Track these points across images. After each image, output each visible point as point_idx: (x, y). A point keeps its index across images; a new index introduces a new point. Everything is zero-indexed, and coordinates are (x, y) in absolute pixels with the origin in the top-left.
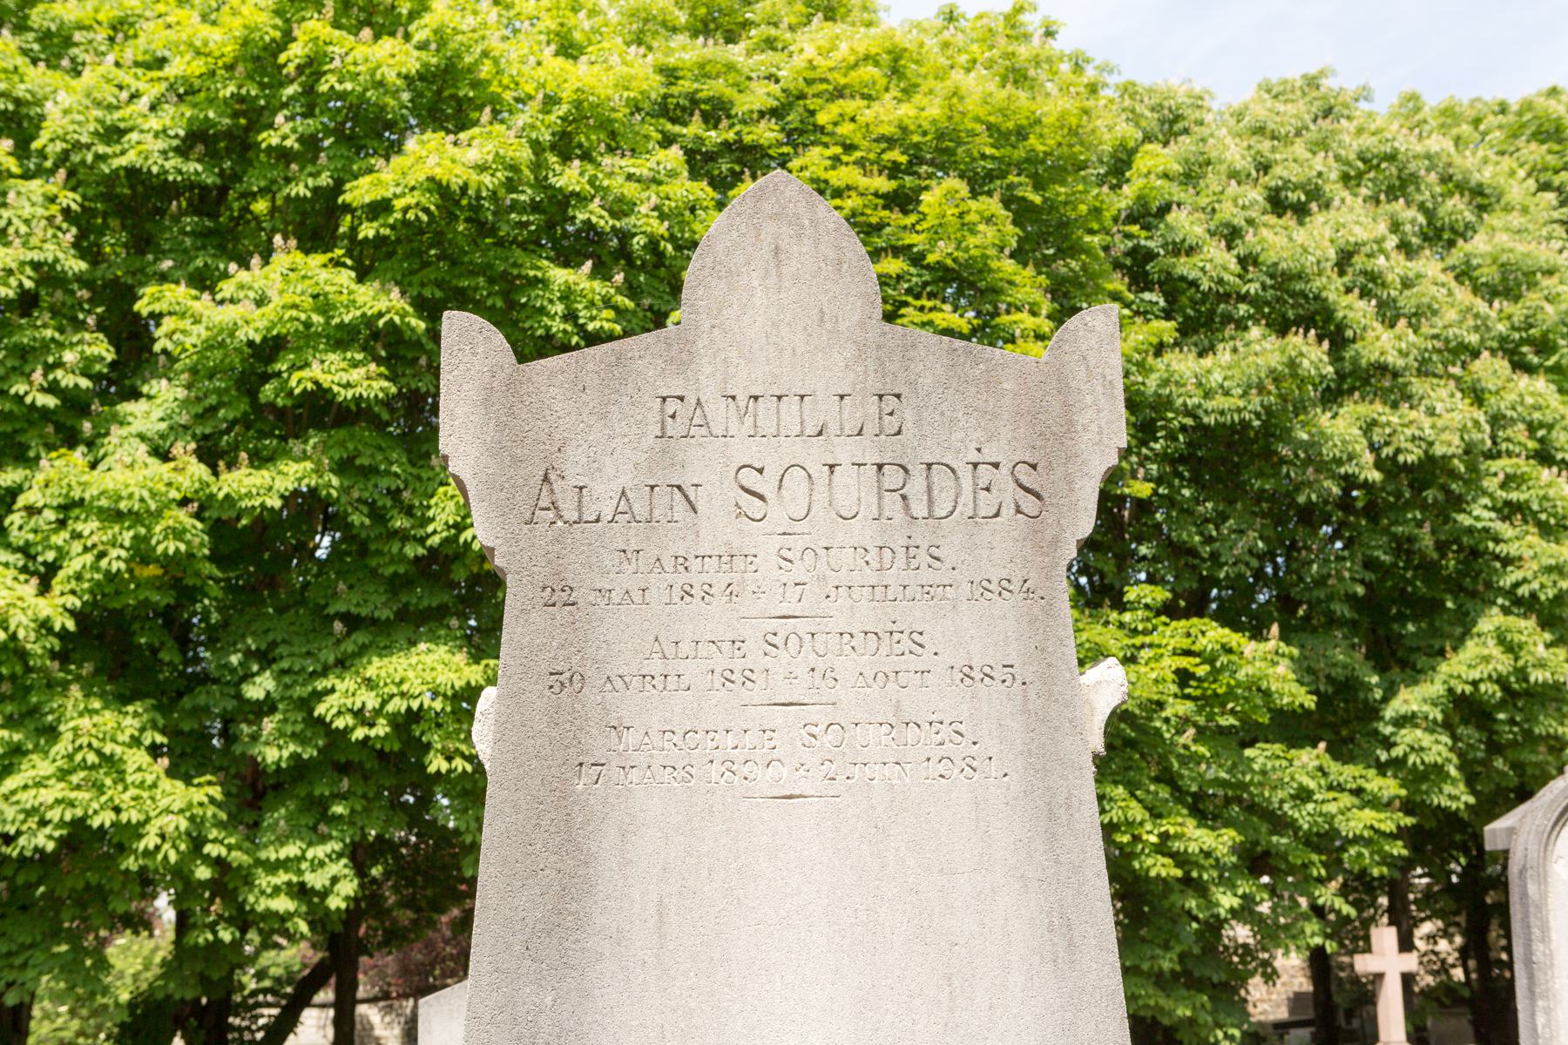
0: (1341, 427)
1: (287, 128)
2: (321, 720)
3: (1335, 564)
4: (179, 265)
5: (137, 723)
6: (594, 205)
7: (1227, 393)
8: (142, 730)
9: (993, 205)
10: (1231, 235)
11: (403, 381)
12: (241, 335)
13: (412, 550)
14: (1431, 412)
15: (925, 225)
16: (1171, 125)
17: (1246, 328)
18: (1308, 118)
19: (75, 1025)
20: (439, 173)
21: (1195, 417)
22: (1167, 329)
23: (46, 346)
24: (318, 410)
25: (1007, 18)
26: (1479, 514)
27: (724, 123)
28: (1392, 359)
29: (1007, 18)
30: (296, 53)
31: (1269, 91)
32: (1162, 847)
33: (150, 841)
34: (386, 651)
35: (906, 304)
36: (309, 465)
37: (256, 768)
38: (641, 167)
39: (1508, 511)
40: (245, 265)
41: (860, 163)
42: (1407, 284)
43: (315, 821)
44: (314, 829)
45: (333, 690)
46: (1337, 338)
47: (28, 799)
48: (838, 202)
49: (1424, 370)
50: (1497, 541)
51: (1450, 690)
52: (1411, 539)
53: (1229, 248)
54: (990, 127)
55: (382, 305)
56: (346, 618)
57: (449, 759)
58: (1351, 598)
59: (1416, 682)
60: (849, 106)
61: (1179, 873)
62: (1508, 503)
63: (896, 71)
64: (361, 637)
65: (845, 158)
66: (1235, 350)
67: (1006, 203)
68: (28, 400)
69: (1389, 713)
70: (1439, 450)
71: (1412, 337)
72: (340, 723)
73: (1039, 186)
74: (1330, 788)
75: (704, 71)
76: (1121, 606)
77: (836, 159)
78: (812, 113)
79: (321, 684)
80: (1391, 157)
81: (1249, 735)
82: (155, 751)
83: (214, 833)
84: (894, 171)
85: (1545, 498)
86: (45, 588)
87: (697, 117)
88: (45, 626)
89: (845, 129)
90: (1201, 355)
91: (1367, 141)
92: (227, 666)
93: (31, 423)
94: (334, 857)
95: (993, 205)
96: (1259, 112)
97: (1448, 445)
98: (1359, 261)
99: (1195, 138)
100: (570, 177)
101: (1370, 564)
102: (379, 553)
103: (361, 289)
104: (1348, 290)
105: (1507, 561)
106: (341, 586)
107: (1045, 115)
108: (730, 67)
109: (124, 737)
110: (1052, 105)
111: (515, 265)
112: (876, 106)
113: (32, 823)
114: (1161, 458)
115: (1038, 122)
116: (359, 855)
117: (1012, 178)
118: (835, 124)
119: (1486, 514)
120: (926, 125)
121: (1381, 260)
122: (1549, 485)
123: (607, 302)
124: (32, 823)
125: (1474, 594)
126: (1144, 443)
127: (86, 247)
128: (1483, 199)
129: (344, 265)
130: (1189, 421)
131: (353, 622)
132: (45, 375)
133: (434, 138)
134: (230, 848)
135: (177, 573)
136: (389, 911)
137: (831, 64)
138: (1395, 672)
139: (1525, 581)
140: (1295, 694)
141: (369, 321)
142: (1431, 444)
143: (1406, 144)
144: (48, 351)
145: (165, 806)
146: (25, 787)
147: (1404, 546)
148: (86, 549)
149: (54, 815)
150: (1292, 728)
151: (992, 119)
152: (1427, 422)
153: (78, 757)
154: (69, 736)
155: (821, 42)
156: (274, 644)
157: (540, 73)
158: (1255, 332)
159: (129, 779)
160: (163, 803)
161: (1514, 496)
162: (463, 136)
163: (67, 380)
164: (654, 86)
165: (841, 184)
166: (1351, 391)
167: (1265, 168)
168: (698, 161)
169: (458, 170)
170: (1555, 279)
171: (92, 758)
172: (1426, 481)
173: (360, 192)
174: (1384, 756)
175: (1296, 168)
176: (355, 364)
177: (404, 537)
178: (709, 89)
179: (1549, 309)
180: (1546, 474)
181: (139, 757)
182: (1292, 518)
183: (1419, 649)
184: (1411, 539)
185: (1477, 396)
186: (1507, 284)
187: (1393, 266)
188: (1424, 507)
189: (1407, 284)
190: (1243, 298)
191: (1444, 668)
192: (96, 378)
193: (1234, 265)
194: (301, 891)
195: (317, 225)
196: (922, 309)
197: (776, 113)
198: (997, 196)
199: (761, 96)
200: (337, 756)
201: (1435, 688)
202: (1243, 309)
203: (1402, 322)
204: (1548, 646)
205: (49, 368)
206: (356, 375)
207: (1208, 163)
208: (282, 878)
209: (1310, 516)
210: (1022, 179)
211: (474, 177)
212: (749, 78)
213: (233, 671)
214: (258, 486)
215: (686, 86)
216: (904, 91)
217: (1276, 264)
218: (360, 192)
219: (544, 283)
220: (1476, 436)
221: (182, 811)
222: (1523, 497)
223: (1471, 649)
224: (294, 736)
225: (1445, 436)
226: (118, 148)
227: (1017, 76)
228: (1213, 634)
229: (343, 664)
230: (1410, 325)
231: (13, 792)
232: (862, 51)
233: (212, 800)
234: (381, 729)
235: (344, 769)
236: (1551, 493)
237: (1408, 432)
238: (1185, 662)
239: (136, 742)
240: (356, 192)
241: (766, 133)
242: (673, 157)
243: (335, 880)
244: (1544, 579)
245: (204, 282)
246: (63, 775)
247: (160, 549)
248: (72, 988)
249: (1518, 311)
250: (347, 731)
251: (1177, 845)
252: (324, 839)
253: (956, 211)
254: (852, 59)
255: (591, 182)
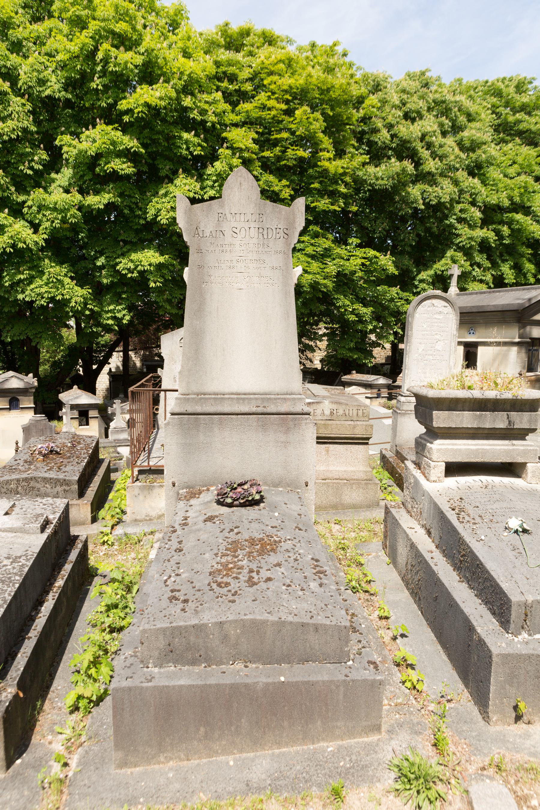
0: (415, 191)
1: (98, 82)
2: (118, 271)
3: (409, 233)
4: (67, 129)
5: (66, 270)
6: (195, 112)
7: (382, 179)
8: (67, 272)
9: (318, 115)
10: (390, 127)
11: (138, 168)
12: (89, 153)
13: (142, 222)
14: (442, 188)
15: (296, 121)
16: (377, 88)
17: (390, 159)
18: (419, 87)
19: (48, 355)
20: (148, 100)
21: (373, 187)
22: (366, 158)
23: (28, 154)
24: (114, 177)
25: (331, 47)
26: (452, 220)
27: (235, 83)
28: (433, 170)
29: (331, 47)
30: (100, 55)
31: (409, 76)
32: (352, 313)
33: (73, 304)
34: (135, 251)
35: (289, 148)
36: (112, 195)
37: (100, 283)
38: (209, 98)
39: (460, 220)
40: (87, 129)
41: (277, 99)
42: (441, 146)
43: (118, 300)
44: (118, 301)
45: (121, 262)
46: (417, 164)
47: (37, 290)
48: (269, 112)
49: (442, 175)
50: (456, 229)
51: (436, 273)
52: (431, 228)
53: (388, 132)
54: (318, 88)
55: (131, 145)
56: (123, 241)
57: (155, 283)
58: (411, 246)
59: (426, 270)
60: (275, 78)
61: (357, 319)
62: (460, 218)
63: (289, 66)
64: (128, 247)
65: (272, 97)
66: (386, 166)
67: (322, 114)
68: (25, 172)
69: (418, 278)
70: (443, 200)
71: (440, 164)
72: (124, 272)
73: (332, 109)
74: (399, 298)
75: (230, 64)
76: (346, 244)
77: (269, 97)
78: (262, 80)
79: (118, 260)
80: (444, 102)
81: (379, 282)
82: (72, 278)
83: (90, 302)
84: (287, 102)
85: (472, 216)
86: (36, 232)
87: (226, 80)
88: (36, 243)
89: (273, 87)
90: (376, 167)
91: (437, 96)
92: (90, 255)
93: (26, 179)
94: (124, 309)
95: (318, 115)
96: (404, 84)
97: (446, 199)
98: (427, 138)
99: (384, 92)
100: (187, 101)
101: (418, 235)
102: (132, 222)
103: (124, 137)
104: (423, 147)
105: (458, 235)
106: (122, 232)
107: (336, 84)
108: (238, 62)
109: (62, 274)
110: (338, 80)
111: (171, 131)
112: (283, 79)
113: (39, 298)
114: (362, 199)
115: (333, 87)
116: (130, 308)
117: (324, 106)
118: (270, 84)
119: (454, 221)
120: (298, 86)
121: (434, 138)
122: (473, 212)
123: (199, 145)
124: (39, 298)
125: (447, 245)
126: (356, 194)
127: (37, 122)
128: (470, 118)
129: (118, 130)
130: (370, 188)
131: (126, 242)
132: (29, 164)
133: (145, 86)
134: (94, 306)
135: (75, 228)
136: (136, 325)
137: (269, 63)
138: (421, 267)
139: (462, 242)
140: (392, 269)
141: (128, 150)
142: (440, 198)
143: (449, 97)
144: (30, 156)
145: (77, 294)
146: (36, 287)
147: (428, 230)
148: (48, 220)
149: (46, 295)
150: (391, 280)
151: (319, 85)
152: (440, 191)
153: (51, 280)
154: (47, 273)
155: (266, 54)
156: (103, 249)
157: (178, 65)
158: (393, 160)
159: (66, 287)
160: (76, 294)
161: (463, 216)
162: (154, 86)
163: (36, 167)
164: (212, 69)
165: (271, 106)
166: (419, 181)
167: (404, 104)
168: (227, 96)
169: (154, 100)
170: (486, 146)
171: (55, 280)
172: (438, 210)
173: (123, 105)
174: (415, 291)
175: (414, 105)
176: (124, 163)
177: (139, 217)
178: (231, 70)
179: (484, 156)
180: (473, 209)
181: (67, 280)
182: (397, 221)
183: (429, 260)
184: (431, 228)
185: (456, 183)
186: (472, 147)
187: (437, 140)
188: (436, 218)
189: (441, 146)
190: (390, 149)
191: (435, 266)
192: (43, 165)
193: (389, 137)
194: (114, 318)
195: (111, 116)
196: (293, 150)
197: (251, 79)
198: (320, 112)
199: (245, 74)
200: (122, 282)
201: (431, 272)
202: (390, 152)
203: (437, 159)
204: (464, 261)
205: (30, 162)
206: (124, 166)
207: (386, 102)
208: (110, 315)
209: (404, 220)
210: (328, 107)
211: (159, 102)
212: (243, 66)
213: (92, 256)
214: (97, 201)
215: (224, 69)
216: (292, 74)
217: (402, 137)
218: (123, 105)
219: (180, 138)
220: (454, 196)
221: (81, 296)
222: (465, 216)
223: (443, 261)
224: (111, 275)
225: (445, 196)
226: (44, 88)
227: (329, 70)
228: (372, 253)
229: (123, 255)
230: (439, 159)
231: (33, 289)
232: (279, 58)
233: (89, 292)
234: (135, 275)
235: (124, 284)
236: (474, 215)
237: (434, 194)
238: (363, 261)
239: (66, 275)
240: (122, 106)
241: (248, 87)
242: (219, 95)
243: (124, 315)
244: (467, 242)
245: (77, 135)
246: (47, 284)
247: (70, 221)
248: (54, 344)
249: (473, 156)
250: (126, 274)
251: (356, 312)
252: (121, 304)
253: (306, 117)
254: (276, 61)
255: (194, 103)
